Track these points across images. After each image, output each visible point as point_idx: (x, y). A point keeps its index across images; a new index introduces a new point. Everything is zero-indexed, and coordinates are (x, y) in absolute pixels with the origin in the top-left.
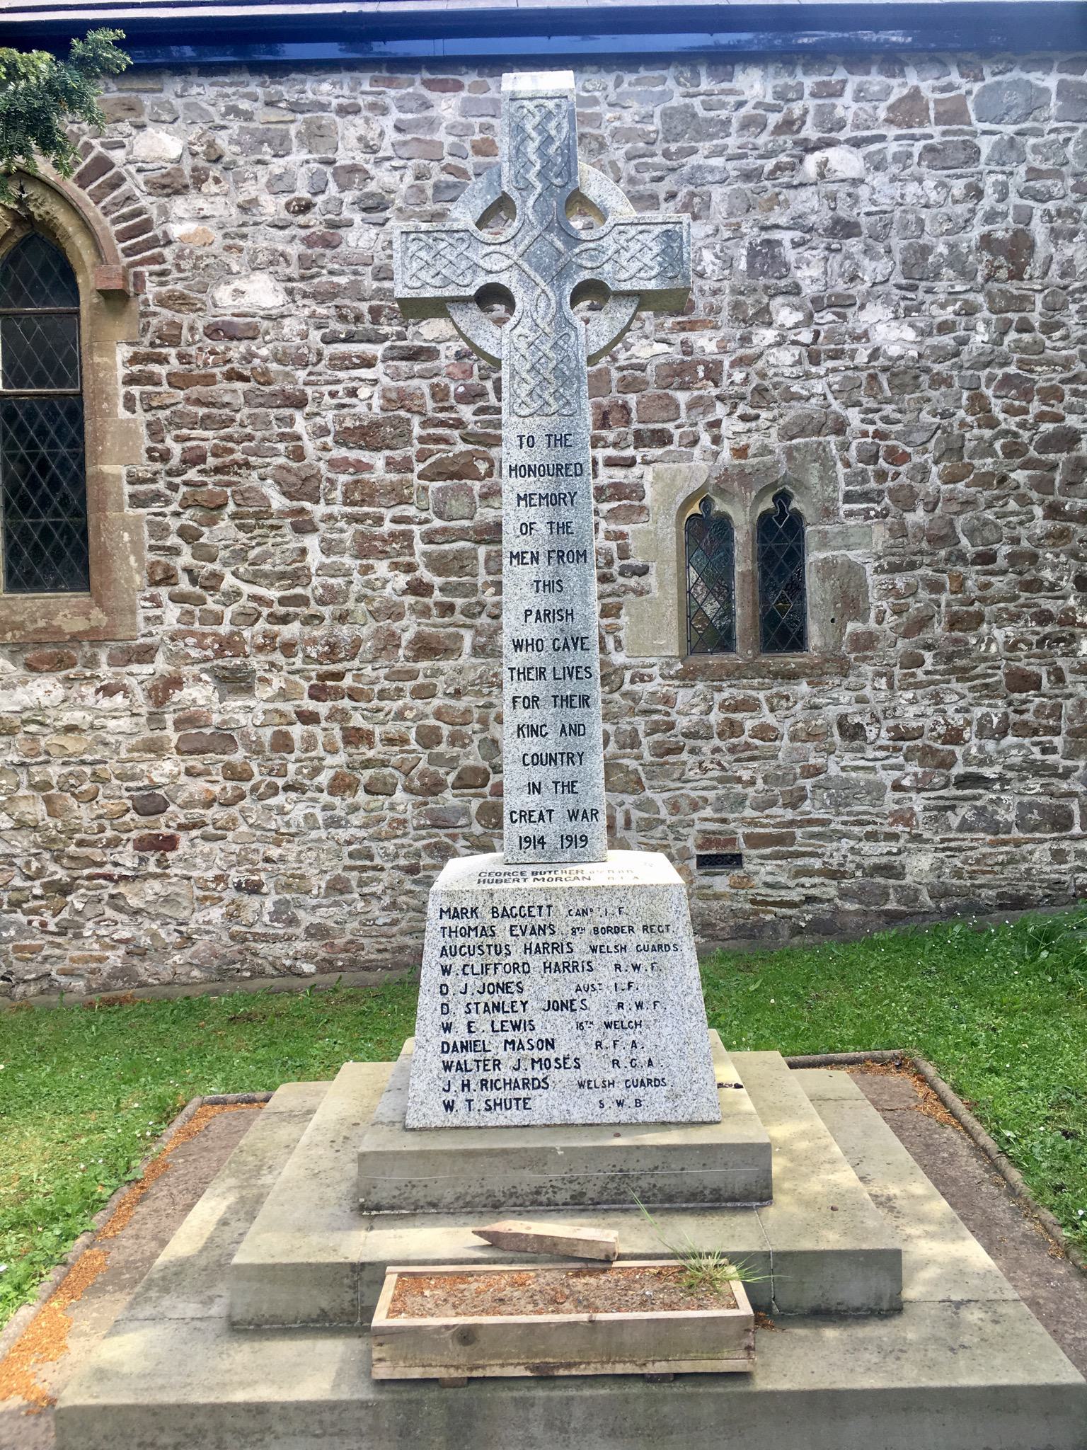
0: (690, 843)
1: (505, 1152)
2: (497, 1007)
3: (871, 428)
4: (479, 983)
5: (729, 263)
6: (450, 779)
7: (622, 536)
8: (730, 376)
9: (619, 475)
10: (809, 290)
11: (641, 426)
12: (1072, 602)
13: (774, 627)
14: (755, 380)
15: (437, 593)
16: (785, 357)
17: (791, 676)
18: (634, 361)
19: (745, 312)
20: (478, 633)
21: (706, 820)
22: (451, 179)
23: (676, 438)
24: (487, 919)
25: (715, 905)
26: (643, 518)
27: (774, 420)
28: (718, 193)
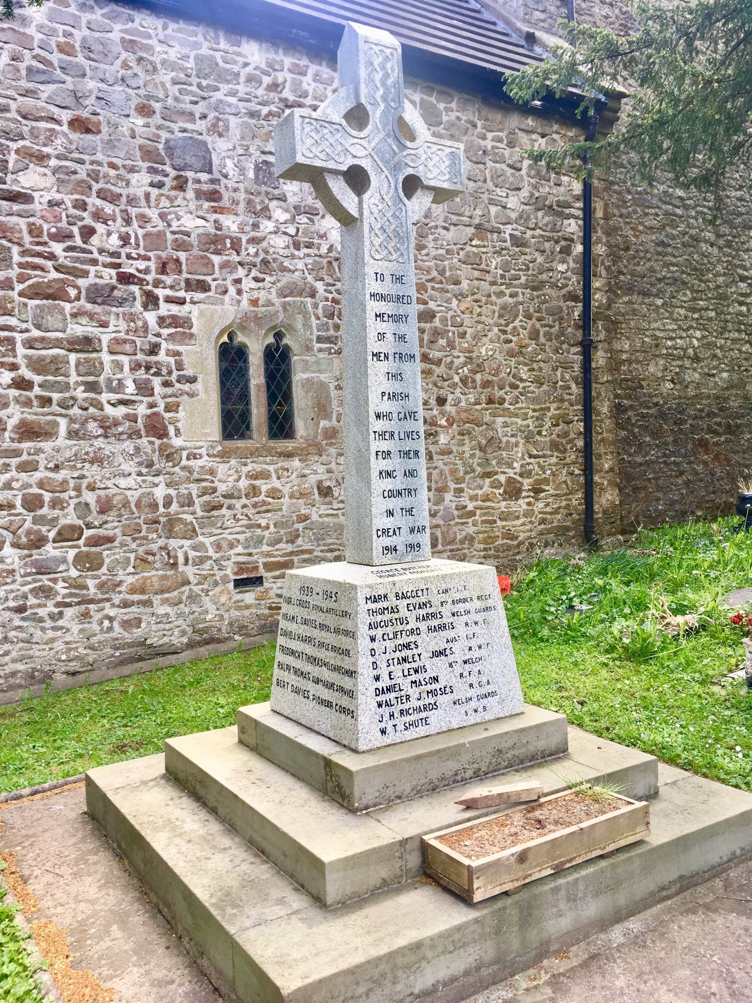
0: (229, 572)
1: (438, 751)
2: (405, 660)
3: (330, 296)
4: (393, 645)
5: (242, 171)
6: (52, 535)
7: (177, 354)
8: (247, 249)
9: (175, 309)
10: (292, 200)
11: (189, 276)
12: (435, 412)
13: (275, 423)
14: (262, 255)
15: (36, 388)
16: (280, 242)
17: (289, 455)
18: (182, 229)
19: (255, 207)
20: (72, 420)
21: (239, 554)
22: (41, 66)
23: (213, 288)
24: (392, 601)
25: (246, 613)
26: (193, 342)
27: (274, 283)
28: (233, 121)
